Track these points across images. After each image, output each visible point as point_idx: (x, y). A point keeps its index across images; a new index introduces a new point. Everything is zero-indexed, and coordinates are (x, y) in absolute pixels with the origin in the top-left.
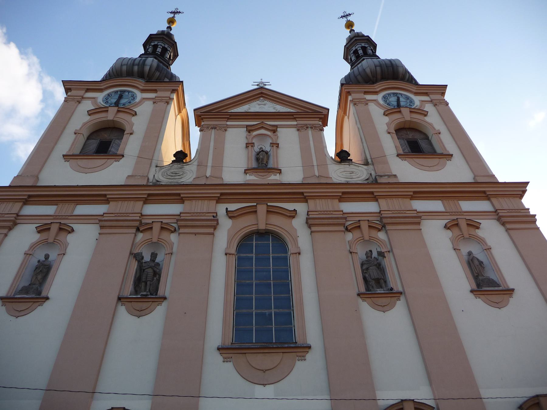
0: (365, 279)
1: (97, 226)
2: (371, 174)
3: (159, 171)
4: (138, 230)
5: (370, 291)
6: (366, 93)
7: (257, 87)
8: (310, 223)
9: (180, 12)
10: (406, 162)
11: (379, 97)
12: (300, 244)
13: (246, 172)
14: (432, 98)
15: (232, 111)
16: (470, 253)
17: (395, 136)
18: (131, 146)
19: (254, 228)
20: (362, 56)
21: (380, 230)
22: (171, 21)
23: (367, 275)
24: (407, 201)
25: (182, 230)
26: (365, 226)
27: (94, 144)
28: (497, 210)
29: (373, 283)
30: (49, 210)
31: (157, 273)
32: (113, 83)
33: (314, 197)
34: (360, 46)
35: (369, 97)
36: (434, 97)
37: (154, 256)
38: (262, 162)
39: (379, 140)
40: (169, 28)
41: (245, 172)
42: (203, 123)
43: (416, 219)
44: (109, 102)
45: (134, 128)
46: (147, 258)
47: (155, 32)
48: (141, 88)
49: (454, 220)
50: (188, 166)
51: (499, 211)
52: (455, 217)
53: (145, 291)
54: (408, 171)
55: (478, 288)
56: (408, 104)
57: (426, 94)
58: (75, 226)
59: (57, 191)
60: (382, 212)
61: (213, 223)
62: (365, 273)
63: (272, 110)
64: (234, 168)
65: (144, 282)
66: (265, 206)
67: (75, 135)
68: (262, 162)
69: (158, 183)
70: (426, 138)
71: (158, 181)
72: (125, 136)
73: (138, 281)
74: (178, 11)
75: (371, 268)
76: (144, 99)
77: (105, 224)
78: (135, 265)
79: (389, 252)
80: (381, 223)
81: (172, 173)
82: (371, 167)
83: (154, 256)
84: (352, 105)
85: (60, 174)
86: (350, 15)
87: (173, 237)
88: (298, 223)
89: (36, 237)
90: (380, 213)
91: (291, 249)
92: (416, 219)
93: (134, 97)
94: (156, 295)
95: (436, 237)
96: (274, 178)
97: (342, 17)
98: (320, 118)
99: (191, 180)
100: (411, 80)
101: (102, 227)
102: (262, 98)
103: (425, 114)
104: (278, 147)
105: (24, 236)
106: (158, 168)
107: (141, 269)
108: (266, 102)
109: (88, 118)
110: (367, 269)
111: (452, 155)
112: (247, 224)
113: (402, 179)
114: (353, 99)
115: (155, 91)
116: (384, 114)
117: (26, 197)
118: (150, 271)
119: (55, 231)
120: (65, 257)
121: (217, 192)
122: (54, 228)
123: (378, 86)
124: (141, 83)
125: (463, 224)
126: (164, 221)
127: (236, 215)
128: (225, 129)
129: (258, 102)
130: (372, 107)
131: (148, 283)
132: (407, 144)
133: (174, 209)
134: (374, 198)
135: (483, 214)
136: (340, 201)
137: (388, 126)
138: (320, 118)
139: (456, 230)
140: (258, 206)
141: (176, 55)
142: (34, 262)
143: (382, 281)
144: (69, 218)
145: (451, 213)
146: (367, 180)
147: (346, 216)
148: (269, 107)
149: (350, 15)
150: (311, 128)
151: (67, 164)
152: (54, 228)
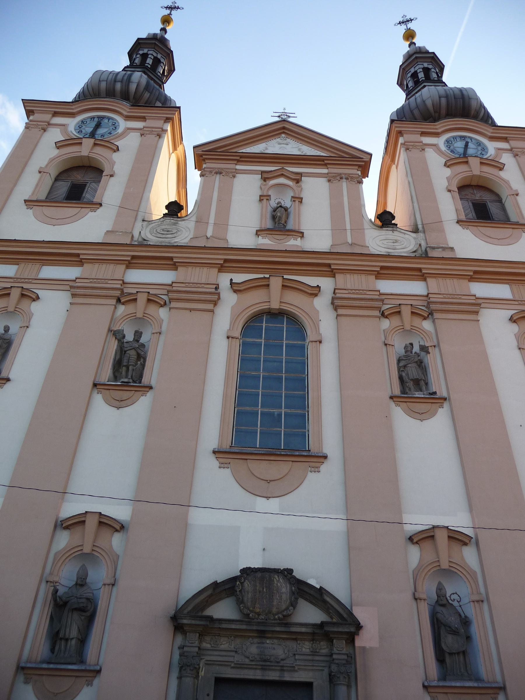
0: (401, 378)
1: (68, 294)
2: (420, 245)
3: (147, 227)
4: (119, 300)
7: (277, 119)
8: (336, 304)
10: (468, 231)
11: (441, 141)
14: (513, 146)
15: (244, 151)
17: (457, 195)
18: (112, 192)
19: (265, 306)
21: (425, 318)
22: (166, 20)
24: (464, 282)
26: (406, 312)
27: (64, 187)
34: (155, 55)
37: (138, 334)
38: (280, 222)
40: (164, 30)
41: (256, 234)
46: (129, 337)
48: (125, 113)
50: (183, 222)
54: (469, 244)
58: (40, 293)
63: (296, 152)
64: (244, 228)
66: (280, 280)
68: (280, 222)
73: (118, 365)
75: (409, 365)
76: (129, 129)
77: (77, 291)
78: (114, 345)
79: (435, 346)
81: (163, 230)
82: (421, 235)
83: (138, 334)
87: (163, 313)
88: (322, 304)
90: (427, 296)
91: (311, 335)
92: (474, 307)
93: (115, 126)
96: (293, 243)
98: (359, 166)
101: (74, 295)
103: (501, 167)
107: (122, 350)
108: (288, 140)
109: (56, 152)
112: (256, 300)
113: (461, 253)
118: (133, 353)
120: (29, 330)
122: (15, 294)
124: (125, 107)
128: (234, 174)
133: (164, 276)
137: (448, 182)
138: (359, 166)
141: (172, 70)
146: (415, 252)
147: (383, 297)
151: (30, 211)
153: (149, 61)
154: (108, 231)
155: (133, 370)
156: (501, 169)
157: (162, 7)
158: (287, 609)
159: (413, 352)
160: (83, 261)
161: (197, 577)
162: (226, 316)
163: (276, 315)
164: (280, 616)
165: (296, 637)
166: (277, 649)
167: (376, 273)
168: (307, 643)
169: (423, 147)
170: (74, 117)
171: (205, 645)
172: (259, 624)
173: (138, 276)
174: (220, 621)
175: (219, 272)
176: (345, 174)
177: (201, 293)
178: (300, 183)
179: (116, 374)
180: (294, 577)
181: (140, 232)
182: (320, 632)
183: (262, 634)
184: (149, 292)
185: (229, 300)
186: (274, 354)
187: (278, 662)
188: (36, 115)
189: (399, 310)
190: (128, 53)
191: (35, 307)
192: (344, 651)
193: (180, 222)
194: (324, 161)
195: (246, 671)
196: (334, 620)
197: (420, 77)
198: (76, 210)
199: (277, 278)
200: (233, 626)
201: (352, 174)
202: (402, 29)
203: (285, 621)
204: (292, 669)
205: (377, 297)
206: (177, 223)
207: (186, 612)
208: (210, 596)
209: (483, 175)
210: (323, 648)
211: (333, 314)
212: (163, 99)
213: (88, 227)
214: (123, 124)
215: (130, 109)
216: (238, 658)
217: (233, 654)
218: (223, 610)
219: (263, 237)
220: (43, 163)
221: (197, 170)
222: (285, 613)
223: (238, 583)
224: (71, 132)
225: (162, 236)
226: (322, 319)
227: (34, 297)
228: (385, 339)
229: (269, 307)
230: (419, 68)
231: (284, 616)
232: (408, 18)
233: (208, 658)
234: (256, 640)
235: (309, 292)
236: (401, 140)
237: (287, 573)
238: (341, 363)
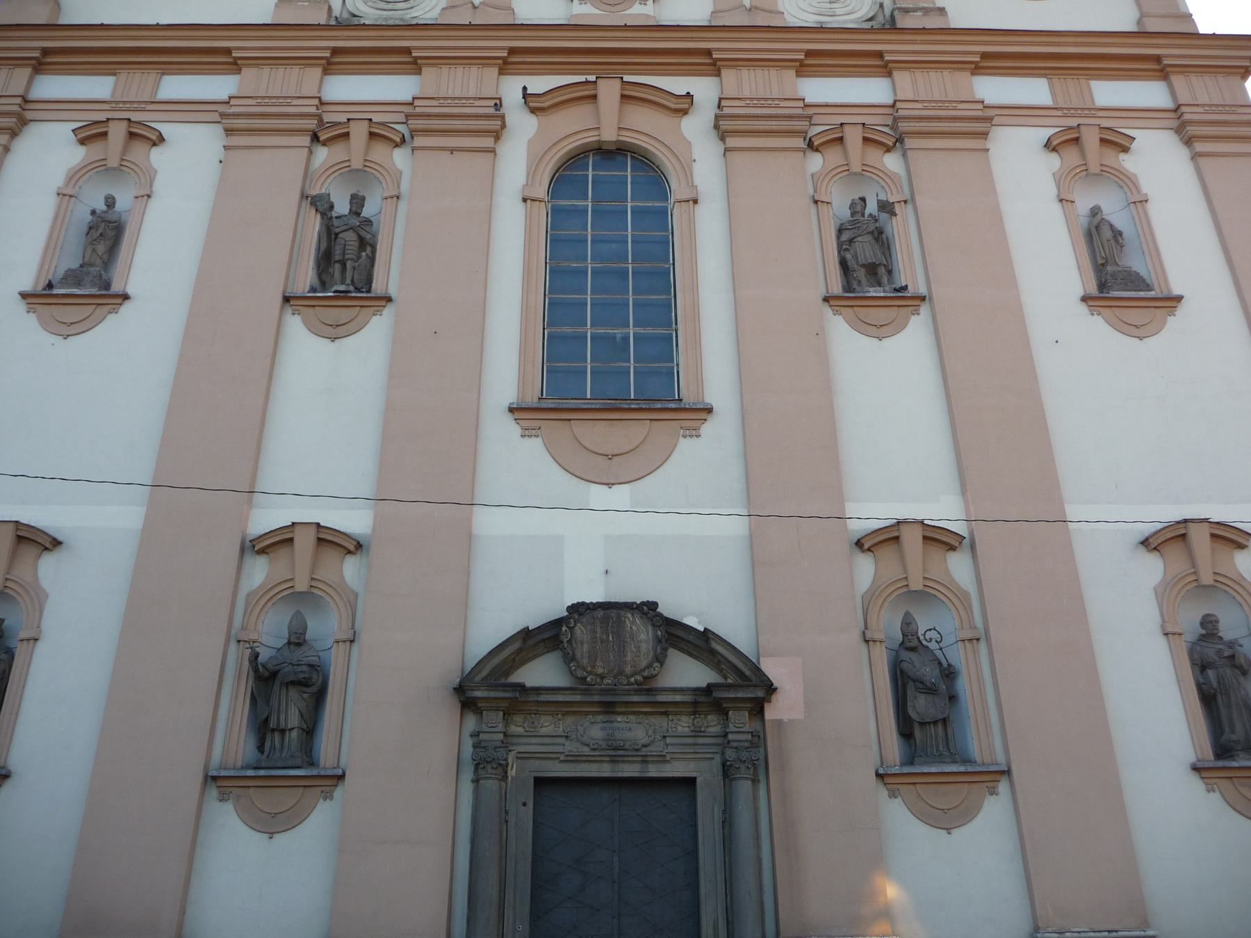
0: (843, 263)
4: (315, 138)
8: (722, 129)
12: (698, 180)
16: (1095, 211)
19: (590, 138)
21: (888, 149)
23: (848, 256)
25: (419, 141)
26: (853, 137)
29: (861, 274)
30: (97, 87)
31: (367, 244)
37: (357, 202)
46: (342, 207)
58: (165, 129)
59: (693, 40)
60: (417, 103)
61: (494, 126)
62: (846, 250)
73: (325, 260)
75: (859, 239)
77: (235, 122)
78: (314, 224)
79: (905, 202)
80: (893, 131)
83: (357, 202)
87: (400, 158)
88: (696, 129)
89: (78, 155)
91: (677, 189)
92: (979, 124)
95: (1022, 168)
101: (229, 131)
105: (49, 155)
107: (330, 233)
112: (574, 127)
118: (350, 237)
121: (500, 45)
131: (349, 264)
133: (394, 88)
139: (1072, 155)
140: (600, 81)
142: (81, 214)
143: (882, 271)
147: (810, 111)
152: (117, 132)
158: (649, 666)
161: (492, 625)
162: (521, 156)
163: (611, 153)
164: (639, 678)
165: (666, 710)
166: (634, 730)
168: (685, 718)
171: (514, 729)
172: (604, 692)
173: (347, 88)
174: (538, 690)
175: (500, 74)
180: (660, 615)
182: (706, 701)
183: (609, 708)
185: (523, 128)
186: (609, 214)
187: (637, 750)
191: (157, 156)
192: (747, 728)
195: (585, 766)
196: (730, 681)
199: (611, 81)
200: (560, 698)
203: (647, 686)
204: (662, 759)
207: (478, 678)
208: (520, 650)
210: (712, 724)
216: (570, 747)
217: (562, 740)
218: (543, 673)
222: (646, 674)
223: (564, 628)
226: (697, 156)
227: (154, 138)
228: (815, 191)
231: (645, 678)
233: (522, 749)
234: (599, 718)
237: (648, 609)
238: (735, 239)
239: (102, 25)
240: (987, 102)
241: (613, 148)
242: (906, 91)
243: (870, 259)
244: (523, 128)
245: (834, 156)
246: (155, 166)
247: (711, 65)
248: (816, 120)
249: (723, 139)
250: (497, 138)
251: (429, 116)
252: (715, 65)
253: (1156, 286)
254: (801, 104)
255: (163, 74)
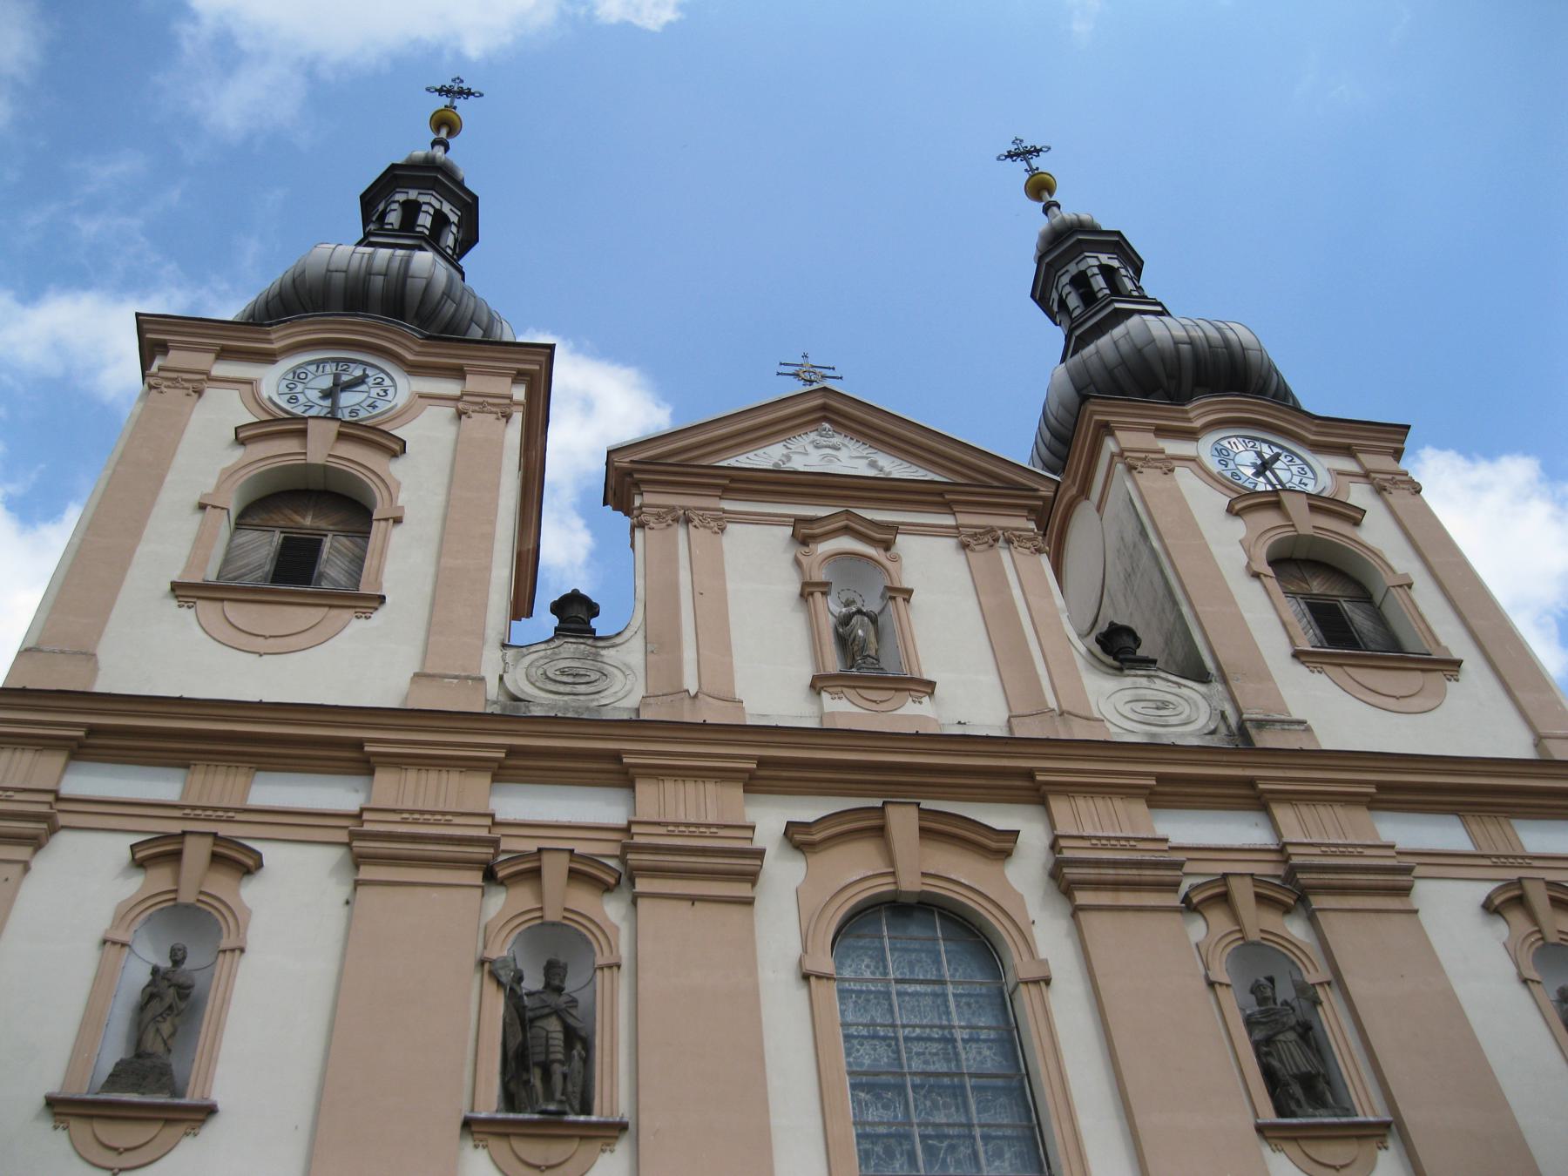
0: (1269, 1075)
1: (335, 854)
2: (1223, 714)
3: (517, 661)
4: (490, 876)
5: (1293, 1115)
6: (1161, 432)
7: (798, 387)
8: (1065, 879)
9: (469, 93)
10: (1323, 676)
11: (1204, 450)
12: (1043, 951)
13: (819, 684)
14: (1124, 445)
15: (732, 462)
17: (1273, 584)
19: (884, 886)
20: (422, 237)
21: (607, 889)
23: (1275, 1063)
24: (1360, 815)
25: (642, 885)
26: (555, 869)
28: (1285, 844)
29: (1296, 1090)
30: (162, 786)
31: (579, 1040)
32: (310, 332)
33: (659, 773)
34: (437, 206)
35: (1172, 447)
36: (1372, 461)
38: (861, 651)
39: (1230, 599)
41: (812, 686)
42: (637, 503)
43: (1392, 881)
44: (302, 399)
45: (402, 499)
47: (400, 160)
49: (167, 837)
50: (612, 652)
51: (1290, 850)
52: (1513, 874)
53: (549, 1096)
54: (1337, 712)
55: (1280, 1112)
56: (1296, 480)
57: (1348, 451)
59: (967, 754)
60: (634, 829)
61: (744, 867)
62: (1268, 1054)
63: (862, 469)
64: (771, 672)
65: (537, 1064)
66: (913, 813)
67: (199, 516)
68: (861, 651)
69: (522, 711)
70: (1364, 596)
71: (516, 699)
72: (377, 528)
73: (519, 1064)
74: (465, 86)
75: (1281, 1037)
76: (422, 396)
77: (368, 850)
78: (497, 1005)
79: (1329, 983)
81: (563, 672)
82: (1218, 687)
84: (1120, 467)
85: (168, 654)
86: (1038, 151)
90: (627, 830)
92: (1392, 881)
94: (586, 1108)
96: (912, 713)
97: (1010, 155)
98: (1031, 509)
99: (633, 701)
100: (1282, 396)
101: (358, 860)
102: (827, 425)
103: (1354, 517)
104: (907, 601)
105: (83, 885)
106: (510, 653)
107: (520, 1017)
108: (837, 440)
110: (1269, 1041)
111: (1458, 663)
112: (855, 870)
113: (1329, 739)
114: (1122, 451)
115: (459, 373)
116: (1230, 510)
117: (81, 733)
118: (554, 1025)
119: (192, 873)
121: (745, 755)
123: (1198, 412)
125: (1539, 898)
126: (580, 848)
127: (817, 837)
128: (721, 522)
129: (813, 436)
130: (1185, 478)
131: (557, 1069)
132: (1307, 611)
133: (597, 808)
134: (1256, 800)
135: (1443, 861)
136: (496, 779)
137: (1247, 551)
138: (1031, 509)
140: (890, 810)
143: (1322, 1086)
144: (239, 817)
145: (1500, 861)
146: (1213, 732)
147: (497, 832)
148: (850, 458)
149: (1038, 151)
150: (1009, 541)
151: (188, 615)
152: (196, 853)
153: (425, 220)
154: (416, 675)
155: (565, 1076)
156: (395, 455)
157: (428, 90)
159: (1279, 1001)
160: (373, 759)
163: (899, 908)
167: (496, 765)
169: (1168, 465)
170: (274, 362)
173: (521, 804)
175: (493, 781)
176: (1004, 529)
177: (704, 852)
178: (894, 550)
179: (512, 1086)
181: (501, 678)
184: (571, 851)
185: (784, 875)
188: (172, 353)
189: (1222, 889)
190: (362, 197)
191: (251, 893)
193: (603, 652)
194: (941, 494)
197: (420, 222)
198: (315, 614)
199: (904, 809)
201: (1017, 529)
202: (1018, 172)
205: (484, 833)
206: (598, 654)
209: (334, 463)
211: (1063, 907)
212: (485, 318)
213: (350, 666)
214: (405, 387)
215: (422, 345)
219: (834, 696)
220: (206, 484)
221: (609, 508)
224: (270, 399)
225: (562, 688)
228: (1207, 968)
229: (891, 887)
230: (430, 202)
232: (1028, 144)
235: (994, 845)
236: (1110, 445)
239: (181, 698)
240: (499, 817)
241: (913, 900)
242: (647, 811)
243: (1305, 1067)
244: (784, 875)
245: (522, 898)
246: (249, 905)
247: (1035, 793)
248: (1188, 868)
249: (357, 866)
250: (754, 884)
251: (656, 849)
252: (1038, 790)
253: (1359, 1111)
254: (488, 821)
255: (258, 770)
